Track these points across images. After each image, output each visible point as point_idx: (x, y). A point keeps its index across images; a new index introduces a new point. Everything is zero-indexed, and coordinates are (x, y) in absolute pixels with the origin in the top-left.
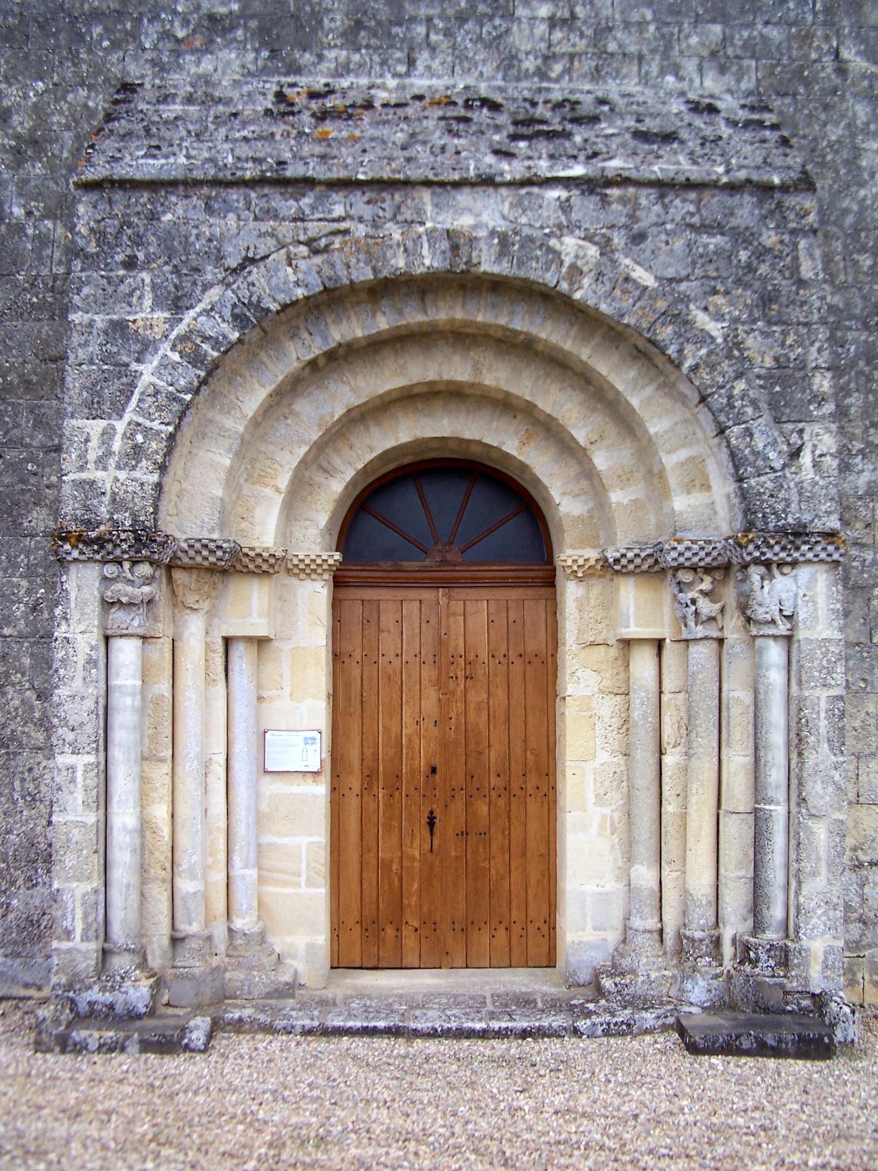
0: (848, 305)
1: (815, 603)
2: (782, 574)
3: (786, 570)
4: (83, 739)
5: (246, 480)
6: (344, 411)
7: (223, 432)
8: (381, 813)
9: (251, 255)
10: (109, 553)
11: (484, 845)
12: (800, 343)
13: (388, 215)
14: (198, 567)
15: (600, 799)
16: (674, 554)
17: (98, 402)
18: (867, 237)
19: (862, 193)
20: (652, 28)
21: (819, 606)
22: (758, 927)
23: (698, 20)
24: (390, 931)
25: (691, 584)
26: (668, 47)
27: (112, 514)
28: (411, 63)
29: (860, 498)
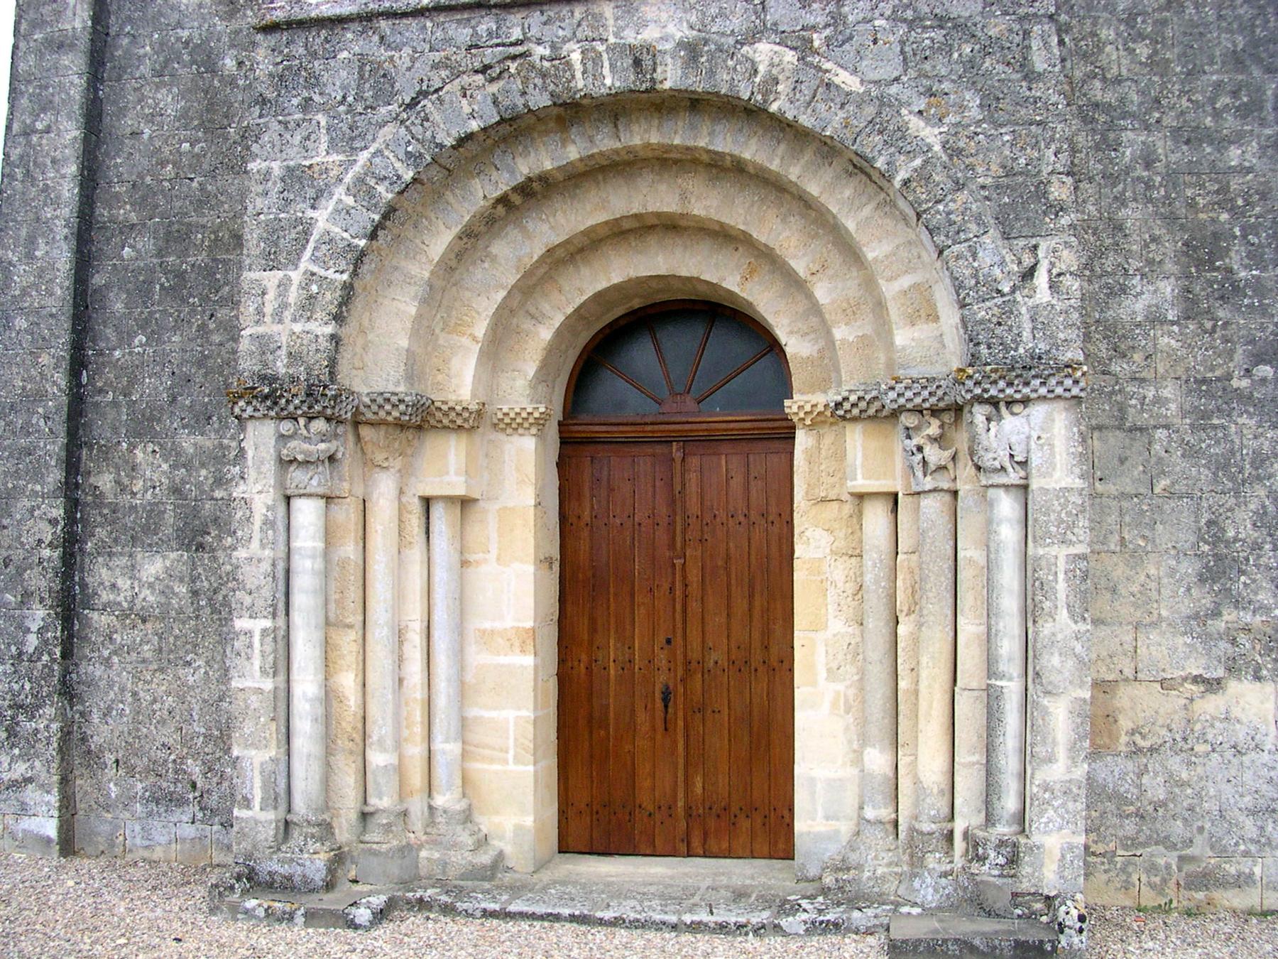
0: (1122, 100)
1: (1052, 446)
2: (1013, 414)
3: (1017, 408)
4: (260, 603)
5: (443, 330)
6: (544, 250)
7: (408, 279)
9: (424, 88)
10: (282, 409)
13: (568, 33)
14: (383, 423)
15: (832, 674)
16: (892, 395)
17: (275, 252)
21: (1057, 450)
22: (990, 820)
25: (918, 428)
29: (1139, 325)
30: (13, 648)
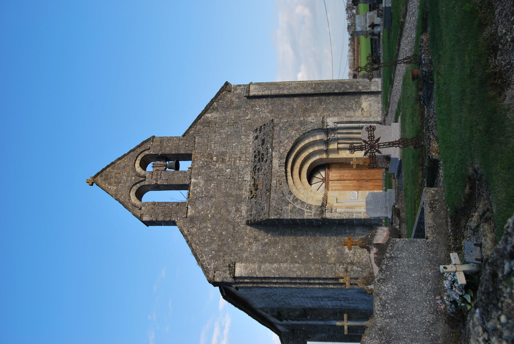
26: (245, 143)
28: (246, 181)
30: (361, 273)
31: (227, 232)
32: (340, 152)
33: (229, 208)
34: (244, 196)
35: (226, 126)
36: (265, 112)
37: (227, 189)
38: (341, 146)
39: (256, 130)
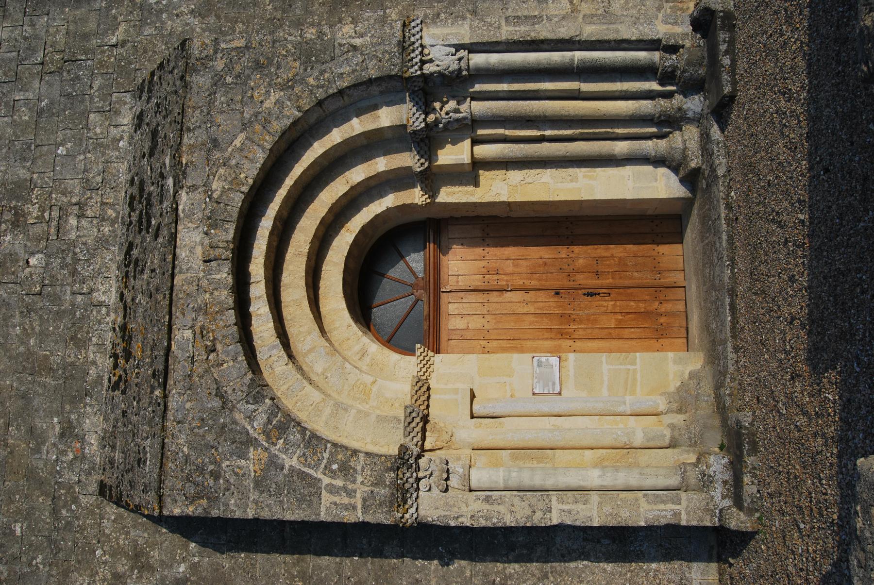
5: (367, 403)
8: (586, 326)
11: (605, 261)
12: (284, 47)
18: (225, 27)
19: (198, 30)
20: (89, 155)
23: (87, 127)
24: (662, 320)
26: (101, 145)
27: (386, 485)
28: (100, 305)
31: (29, 526)
32: (485, 176)
33: (37, 420)
34: (93, 372)
35: (32, 75)
36: (182, 13)
37: (32, 342)
38: (485, 151)
39: (141, 89)
